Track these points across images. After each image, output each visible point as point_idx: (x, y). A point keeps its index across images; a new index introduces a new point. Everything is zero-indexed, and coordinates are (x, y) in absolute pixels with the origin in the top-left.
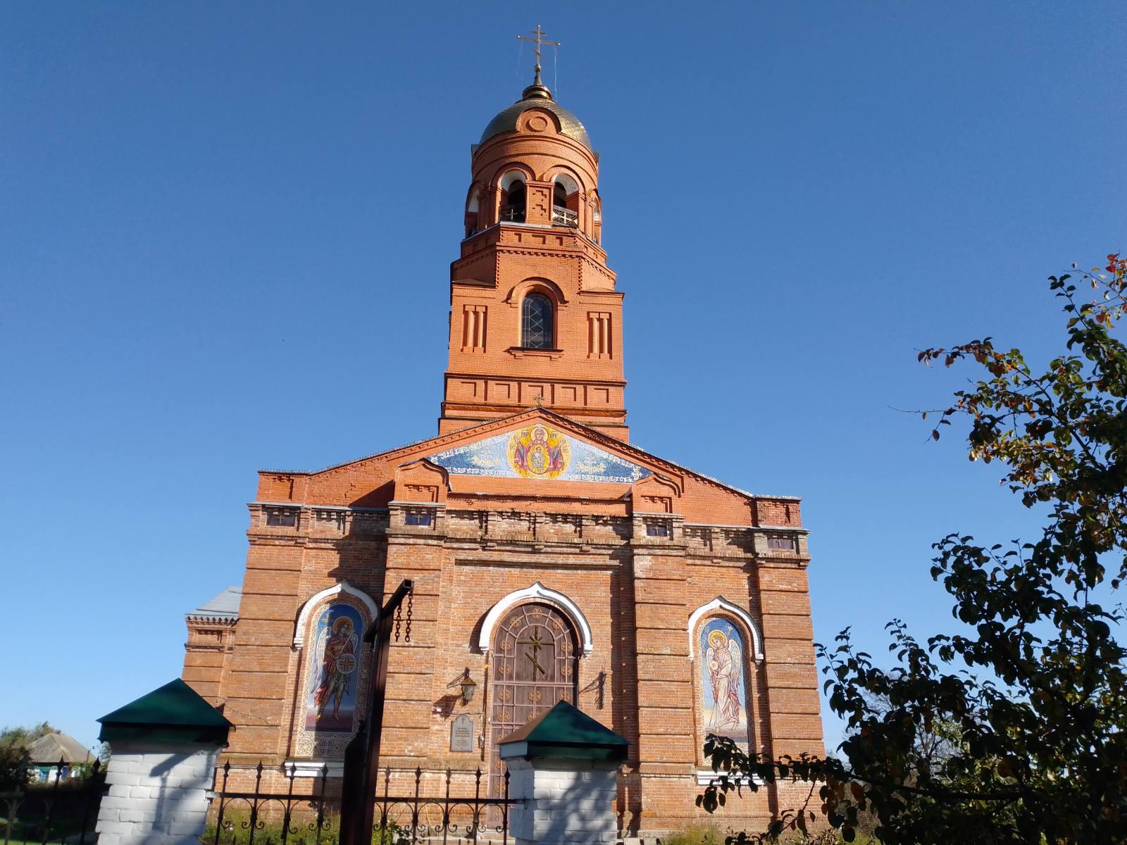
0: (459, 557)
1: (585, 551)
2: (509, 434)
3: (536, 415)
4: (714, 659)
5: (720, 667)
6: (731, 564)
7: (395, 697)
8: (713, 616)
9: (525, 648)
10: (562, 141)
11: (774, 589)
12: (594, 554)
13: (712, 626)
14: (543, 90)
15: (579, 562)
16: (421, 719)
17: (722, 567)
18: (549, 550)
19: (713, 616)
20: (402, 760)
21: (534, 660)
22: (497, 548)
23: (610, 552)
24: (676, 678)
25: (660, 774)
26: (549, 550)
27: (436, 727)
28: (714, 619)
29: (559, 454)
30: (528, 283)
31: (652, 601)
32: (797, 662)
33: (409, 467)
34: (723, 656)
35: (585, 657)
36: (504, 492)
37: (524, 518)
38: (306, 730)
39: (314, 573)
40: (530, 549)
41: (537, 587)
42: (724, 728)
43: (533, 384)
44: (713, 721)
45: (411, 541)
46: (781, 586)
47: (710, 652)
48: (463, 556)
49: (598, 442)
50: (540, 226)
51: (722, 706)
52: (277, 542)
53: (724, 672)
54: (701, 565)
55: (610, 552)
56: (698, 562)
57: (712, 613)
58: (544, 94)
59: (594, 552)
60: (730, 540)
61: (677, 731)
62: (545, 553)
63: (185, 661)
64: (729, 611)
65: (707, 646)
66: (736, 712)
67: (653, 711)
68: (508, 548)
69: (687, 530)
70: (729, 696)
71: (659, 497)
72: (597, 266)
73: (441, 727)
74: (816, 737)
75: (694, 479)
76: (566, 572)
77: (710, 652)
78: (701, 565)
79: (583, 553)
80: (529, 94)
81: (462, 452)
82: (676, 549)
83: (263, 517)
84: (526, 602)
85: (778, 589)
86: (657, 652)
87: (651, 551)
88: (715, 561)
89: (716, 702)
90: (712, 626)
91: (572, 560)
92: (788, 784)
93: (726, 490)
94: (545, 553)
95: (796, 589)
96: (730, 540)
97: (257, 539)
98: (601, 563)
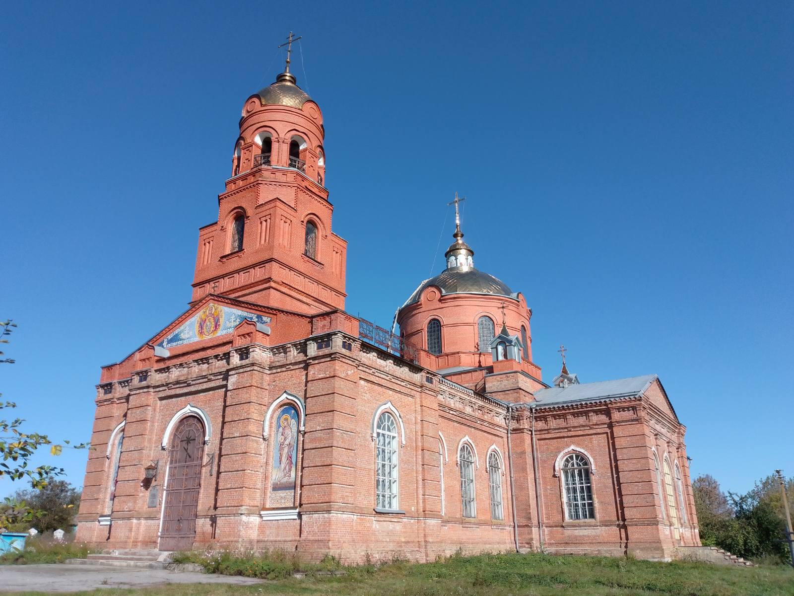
0: (160, 396)
1: (210, 379)
2: (197, 315)
3: (209, 298)
4: (282, 435)
5: (285, 440)
6: (297, 367)
7: (124, 480)
8: (281, 406)
9: (184, 443)
10: (263, 110)
11: (315, 378)
12: (215, 380)
13: (284, 412)
14: (287, 76)
15: (208, 387)
16: (132, 491)
17: (292, 370)
18: (194, 382)
19: (281, 406)
20: (123, 514)
21: (186, 450)
22: (173, 387)
23: (222, 377)
24: (239, 452)
25: (306, 512)
26: (194, 382)
27: (141, 494)
28: (285, 407)
29: (219, 319)
30: (232, 213)
31: (234, 404)
32: (323, 428)
33: (142, 350)
34: (287, 431)
35: (207, 445)
36: (185, 351)
37: (185, 366)
38: (273, 490)
39: (118, 416)
40: (186, 385)
41: (189, 406)
42: (282, 481)
43: (230, 276)
44: (277, 477)
45: (138, 392)
46: (319, 376)
47: (281, 429)
48: (162, 395)
49: (237, 305)
50: (244, 173)
51: (283, 466)
52: (105, 403)
53: (287, 442)
54: (281, 372)
55: (222, 377)
56: (279, 370)
57: (281, 403)
58: (287, 78)
59: (214, 379)
60: (300, 350)
61: (236, 486)
62: (193, 385)
63: (87, 470)
64: (292, 400)
65: (280, 426)
66: (290, 470)
67: (226, 474)
68: (178, 386)
69: (274, 350)
70: (288, 459)
71: (247, 334)
72: (275, 183)
73: (144, 495)
74: (327, 482)
75: (282, 314)
76: (205, 394)
77: (281, 429)
78: (281, 372)
79: (210, 380)
80: (281, 79)
81: (177, 333)
82: (249, 367)
83: (101, 391)
84: (185, 416)
85: (318, 378)
86: (233, 436)
87: (237, 371)
88: (287, 367)
89: (280, 464)
90: (284, 412)
91: (205, 386)
92: (309, 517)
93: (302, 317)
94: (193, 385)
95: (328, 376)
96: (300, 350)
97: (100, 403)
98: (218, 384)
